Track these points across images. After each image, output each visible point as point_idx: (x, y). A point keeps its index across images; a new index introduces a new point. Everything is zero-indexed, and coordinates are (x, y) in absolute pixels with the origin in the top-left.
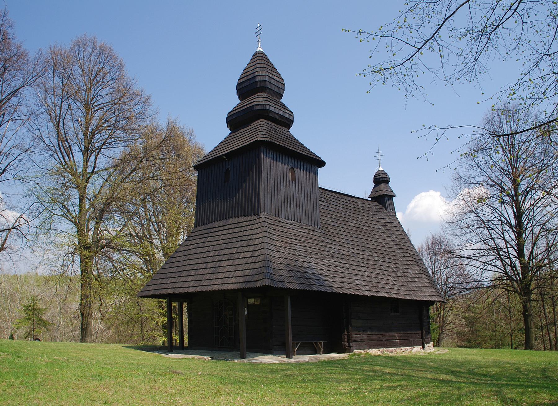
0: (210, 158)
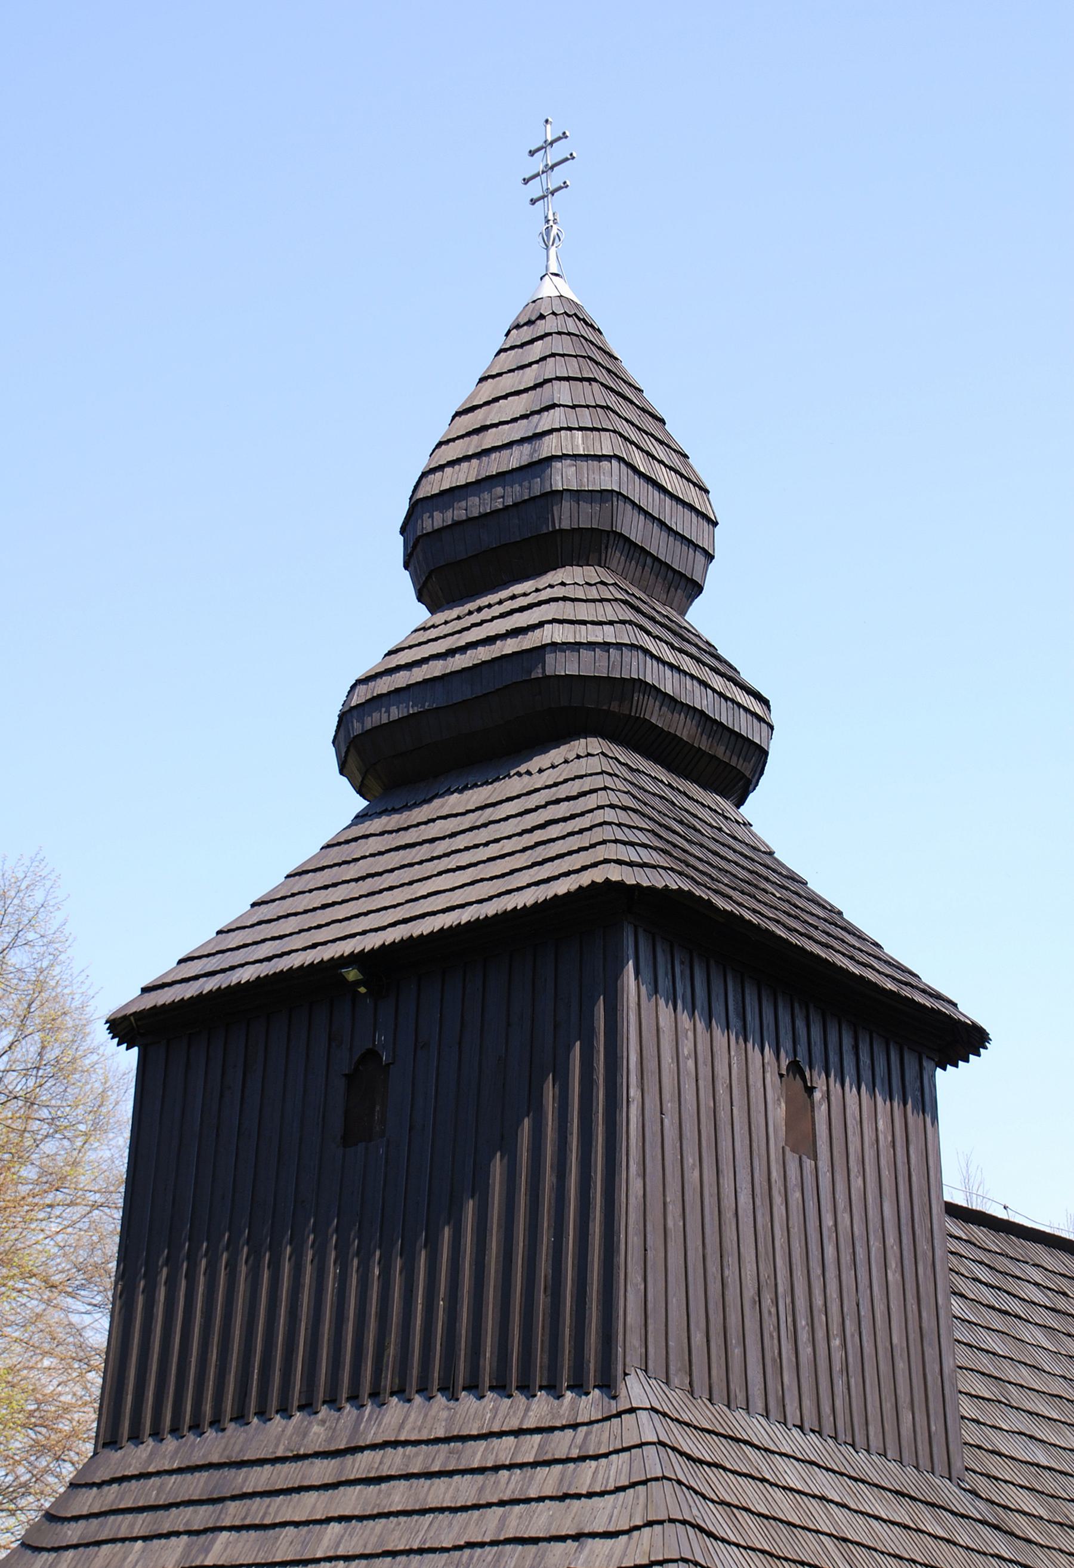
0: (246, 975)
